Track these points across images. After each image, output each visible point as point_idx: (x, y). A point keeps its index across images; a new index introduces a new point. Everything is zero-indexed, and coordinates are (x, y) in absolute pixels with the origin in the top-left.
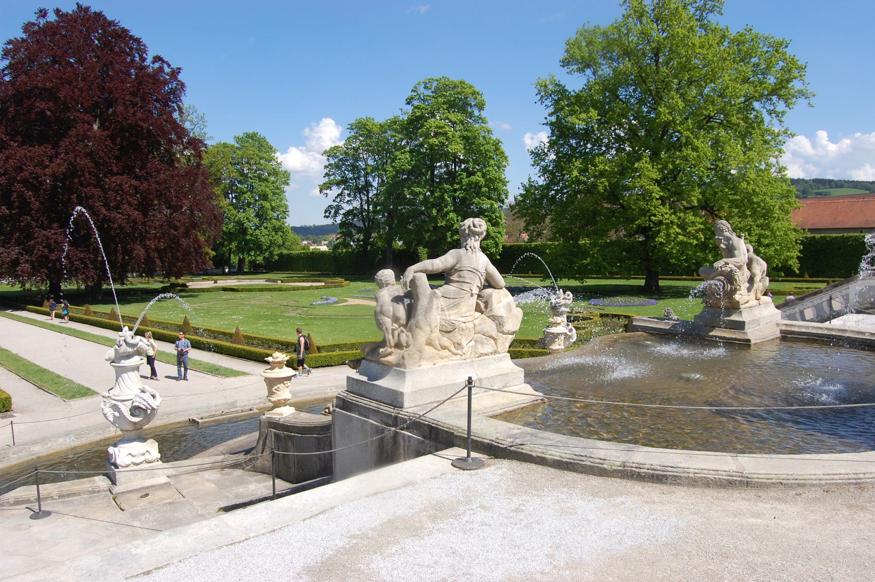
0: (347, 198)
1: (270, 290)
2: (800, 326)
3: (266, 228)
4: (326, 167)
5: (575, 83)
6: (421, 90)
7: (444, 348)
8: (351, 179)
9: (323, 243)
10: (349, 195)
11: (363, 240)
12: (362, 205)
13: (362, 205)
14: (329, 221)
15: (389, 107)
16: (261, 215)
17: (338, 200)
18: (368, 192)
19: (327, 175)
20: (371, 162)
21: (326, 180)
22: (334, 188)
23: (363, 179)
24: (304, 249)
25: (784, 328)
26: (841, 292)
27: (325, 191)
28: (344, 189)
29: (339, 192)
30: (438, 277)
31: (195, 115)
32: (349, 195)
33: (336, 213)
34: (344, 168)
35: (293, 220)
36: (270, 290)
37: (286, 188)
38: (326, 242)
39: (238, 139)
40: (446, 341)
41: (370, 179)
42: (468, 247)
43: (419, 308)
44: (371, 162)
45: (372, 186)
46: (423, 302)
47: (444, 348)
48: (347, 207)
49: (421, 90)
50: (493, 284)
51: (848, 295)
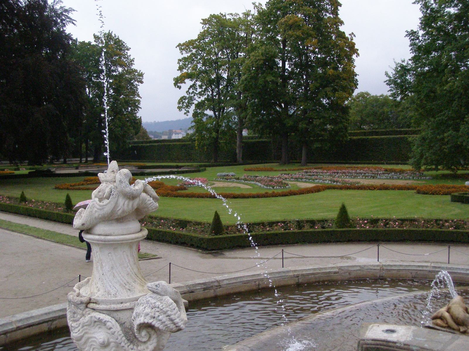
48: (198, 99)
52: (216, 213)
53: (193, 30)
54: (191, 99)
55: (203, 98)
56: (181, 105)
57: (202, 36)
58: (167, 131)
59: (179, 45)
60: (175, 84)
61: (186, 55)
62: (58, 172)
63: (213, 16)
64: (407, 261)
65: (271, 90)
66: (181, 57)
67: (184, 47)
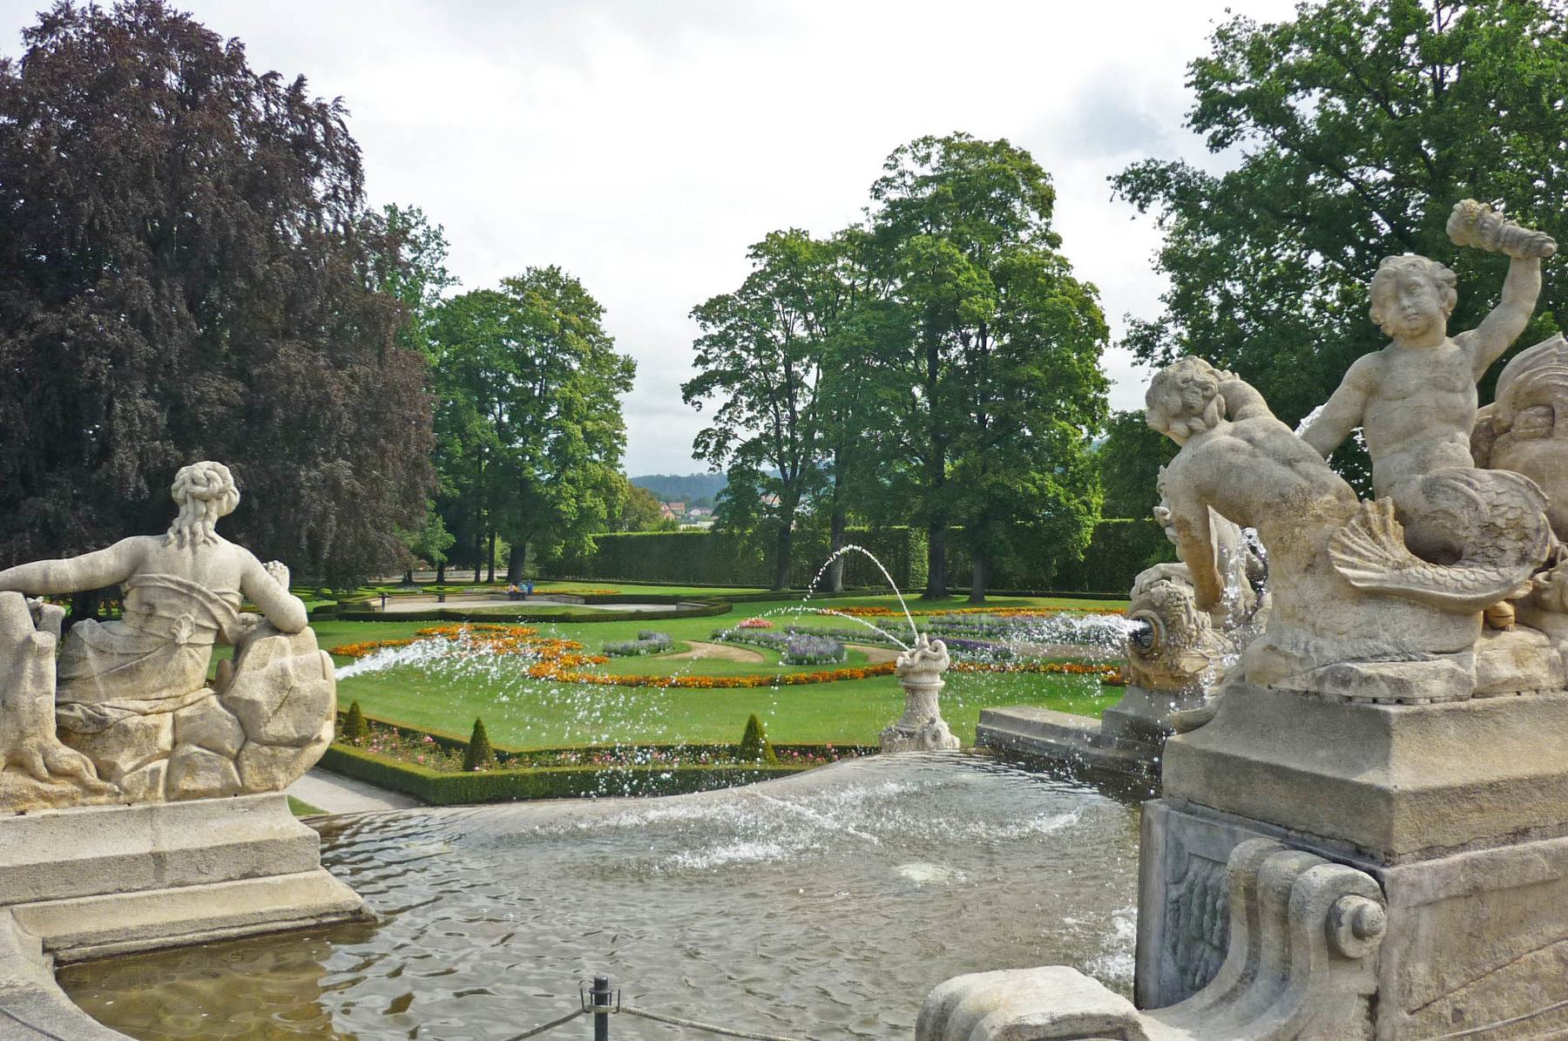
0: (747, 414)
1: (510, 619)
3: (571, 481)
4: (698, 343)
6: (907, 162)
7: (56, 773)
8: (754, 368)
10: (751, 406)
11: (780, 510)
14: (703, 467)
16: (562, 456)
17: (725, 417)
18: (793, 398)
19: (701, 361)
20: (799, 331)
21: (699, 371)
22: (717, 389)
23: (782, 369)
24: (664, 528)
27: (696, 398)
28: (740, 392)
29: (729, 398)
31: (421, 228)
32: (751, 406)
33: (721, 445)
35: (635, 463)
36: (510, 619)
37: (621, 396)
39: (517, 285)
40: (67, 756)
41: (797, 368)
44: (799, 331)
45: (803, 385)
47: (56, 773)
48: (745, 435)
49: (907, 162)
52: (355, 704)
53: (731, 273)
54: (726, 435)
55: (755, 434)
56: (700, 450)
57: (752, 283)
58: (377, 196)
59: (697, 309)
60: (686, 398)
61: (714, 330)
62: (393, 607)
63: (773, 236)
64: (525, 618)
65: (1081, 821)
66: (701, 334)
67: (710, 310)
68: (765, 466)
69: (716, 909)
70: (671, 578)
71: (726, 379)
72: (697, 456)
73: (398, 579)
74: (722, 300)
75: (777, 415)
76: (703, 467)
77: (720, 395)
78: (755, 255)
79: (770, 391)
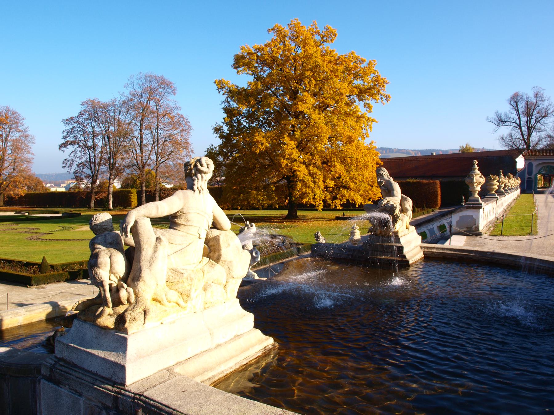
0: (79, 154)
2: (437, 248)
5: (243, 80)
9: (62, 185)
12: (90, 159)
13: (90, 159)
15: (112, 89)
17: (72, 155)
25: (426, 250)
26: (446, 220)
27: (63, 149)
30: (169, 222)
34: (76, 131)
38: (65, 185)
42: (195, 187)
43: (143, 258)
46: (147, 251)
48: (78, 161)
50: (219, 227)
51: (451, 222)
54: (73, 161)
56: (64, 165)
67: (68, 121)
68: (85, 170)
69: (384, 376)
70: (16, 206)
71: (73, 143)
72: (64, 167)
73: (285, 213)
74: (72, 118)
75: (90, 155)
76: (66, 170)
77: (70, 148)
78: (82, 105)
79: (87, 147)
